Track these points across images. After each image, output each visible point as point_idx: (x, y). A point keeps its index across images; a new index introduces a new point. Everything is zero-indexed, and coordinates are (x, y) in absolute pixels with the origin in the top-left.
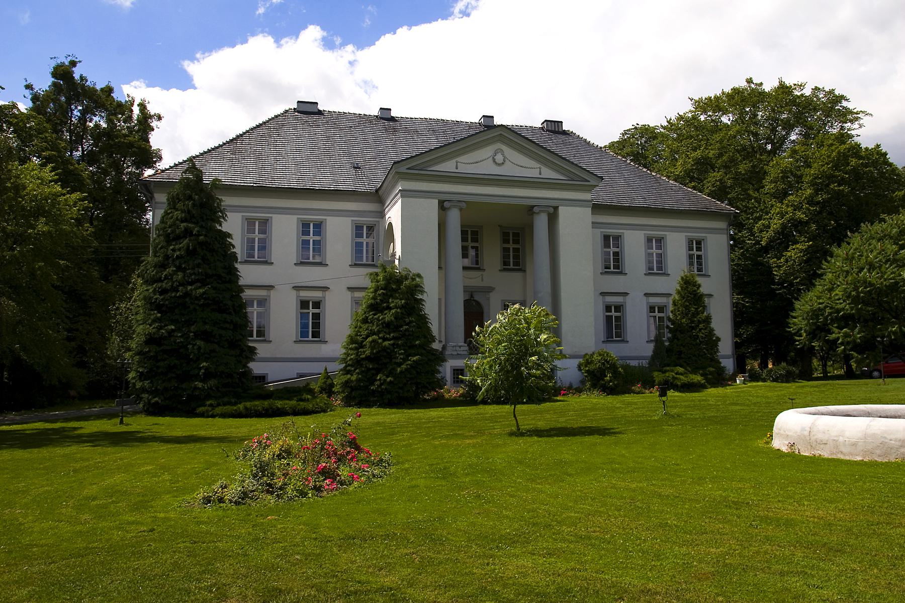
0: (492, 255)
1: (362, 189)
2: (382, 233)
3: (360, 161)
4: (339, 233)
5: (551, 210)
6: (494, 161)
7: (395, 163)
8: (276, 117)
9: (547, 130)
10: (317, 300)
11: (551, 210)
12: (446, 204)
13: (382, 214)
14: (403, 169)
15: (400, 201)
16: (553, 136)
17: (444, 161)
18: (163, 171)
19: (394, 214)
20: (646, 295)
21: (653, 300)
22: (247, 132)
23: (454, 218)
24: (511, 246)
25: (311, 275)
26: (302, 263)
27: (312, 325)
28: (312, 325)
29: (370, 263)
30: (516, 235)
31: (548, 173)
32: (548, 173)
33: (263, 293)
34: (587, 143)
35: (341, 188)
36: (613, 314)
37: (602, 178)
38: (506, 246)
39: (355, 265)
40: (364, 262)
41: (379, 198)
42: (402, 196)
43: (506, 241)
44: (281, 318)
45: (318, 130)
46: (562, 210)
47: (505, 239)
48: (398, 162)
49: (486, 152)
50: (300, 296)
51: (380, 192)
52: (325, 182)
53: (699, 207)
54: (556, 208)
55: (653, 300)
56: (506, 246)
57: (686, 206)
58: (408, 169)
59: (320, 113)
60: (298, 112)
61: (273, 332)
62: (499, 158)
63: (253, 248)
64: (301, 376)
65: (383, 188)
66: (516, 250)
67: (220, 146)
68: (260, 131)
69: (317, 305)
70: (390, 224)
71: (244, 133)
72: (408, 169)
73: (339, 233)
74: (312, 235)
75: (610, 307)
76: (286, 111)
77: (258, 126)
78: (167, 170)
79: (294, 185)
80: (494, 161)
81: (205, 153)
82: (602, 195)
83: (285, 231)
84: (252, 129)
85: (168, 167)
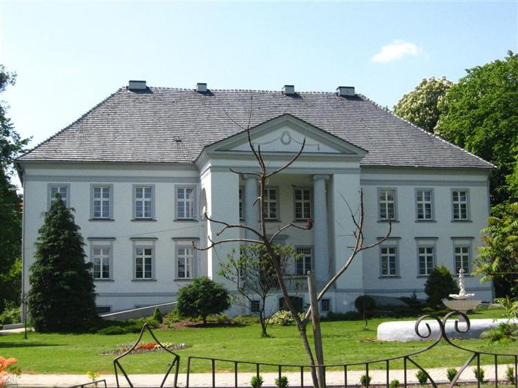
0: (287, 210)
1: (182, 160)
2: (198, 193)
3: (180, 134)
4: (165, 198)
5: (328, 177)
6: (282, 141)
7: (205, 147)
8: (113, 95)
9: (341, 96)
10: (148, 248)
11: (328, 177)
12: (245, 176)
13: (198, 180)
14: (212, 151)
15: (210, 174)
16: (346, 101)
17: (240, 144)
18: (30, 151)
19: (206, 181)
20: (417, 238)
21: (422, 243)
22: (90, 111)
23: (252, 186)
24: (303, 201)
25: (143, 229)
26: (137, 220)
27: (144, 270)
28: (144, 270)
29: (190, 218)
30: (307, 192)
31: (325, 148)
32: (325, 148)
33: (107, 243)
34: (375, 106)
35: (166, 160)
36: (426, 255)
37: (367, 151)
38: (298, 201)
39: (179, 220)
40: (185, 217)
41: (195, 167)
42: (211, 171)
43: (298, 197)
44: (123, 263)
45: (148, 106)
46: (336, 177)
47: (297, 195)
48: (208, 146)
49: (277, 134)
50: (123, 244)
51: (197, 163)
52: (155, 156)
53: (462, 164)
54: (331, 176)
55: (422, 243)
56: (298, 201)
57: (451, 163)
58: (216, 150)
59: (148, 90)
60: (131, 90)
61: (115, 272)
62: (286, 139)
63: (99, 209)
64: (137, 307)
65: (199, 160)
66: (307, 205)
67: (71, 126)
68: (102, 110)
69: (148, 252)
70: (204, 189)
71: (88, 113)
72: (216, 150)
73: (165, 198)
74: (144, 194)
75: (150, 254)
76: (121, 90)
77: (99, 106)
78: (33, 150)
79: (129, 159)
80: (282, 141)
81: (60, 133)
82: (367, 161)
83: (123, 199)
84: (94, 109)
85: (33, 148)
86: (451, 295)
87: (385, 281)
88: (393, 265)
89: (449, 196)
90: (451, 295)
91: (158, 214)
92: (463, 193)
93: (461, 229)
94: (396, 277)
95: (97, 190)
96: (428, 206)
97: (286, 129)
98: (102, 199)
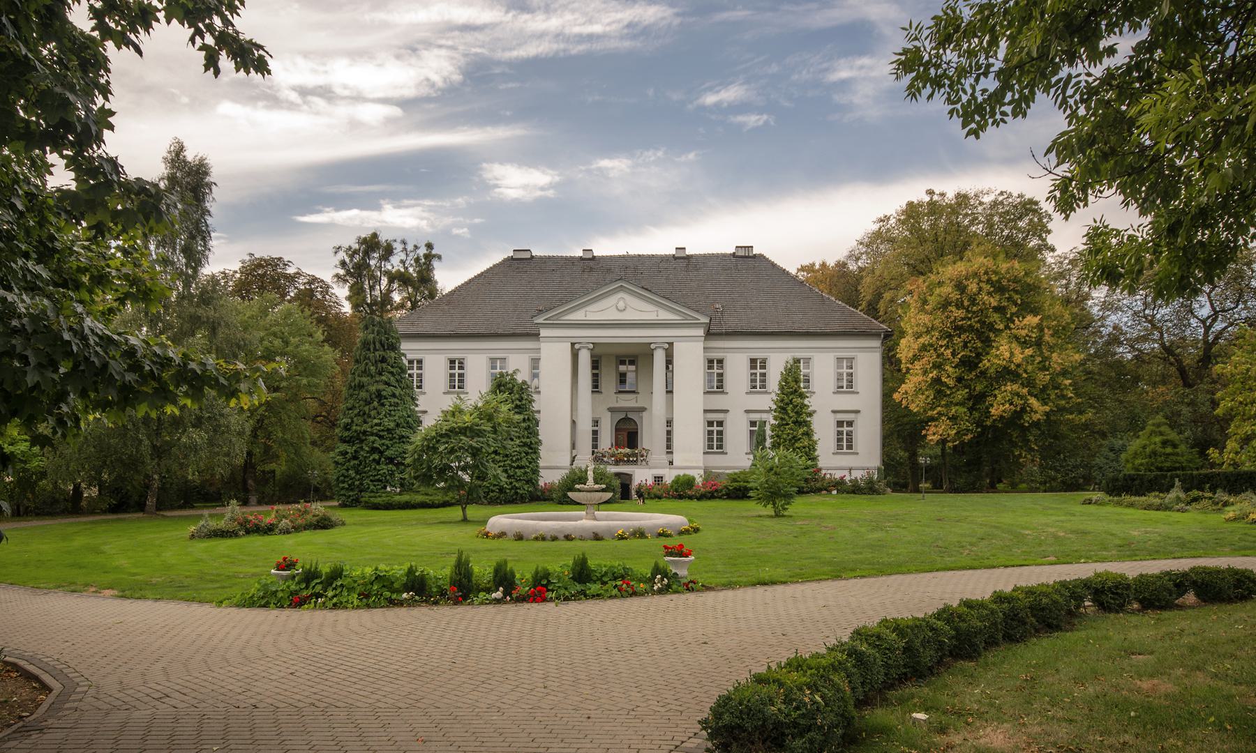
5: (667, 346)
11: (667, 346)
20: (747, 411)
24: (759, 371)
36: (715, 428)
54: (671, 344)
69: (720, 424)
86: (577, 486)
87: (839, 457)
88: (720, 440)
89: (747, 364)
90: (577, 486)
91: (859, 383)
92: (420, 362)
93: (845, 402)
94: (723, 453)
95: (452, 362)
96: (461, 375)
97: (621, 295)
98: (457, 371)
